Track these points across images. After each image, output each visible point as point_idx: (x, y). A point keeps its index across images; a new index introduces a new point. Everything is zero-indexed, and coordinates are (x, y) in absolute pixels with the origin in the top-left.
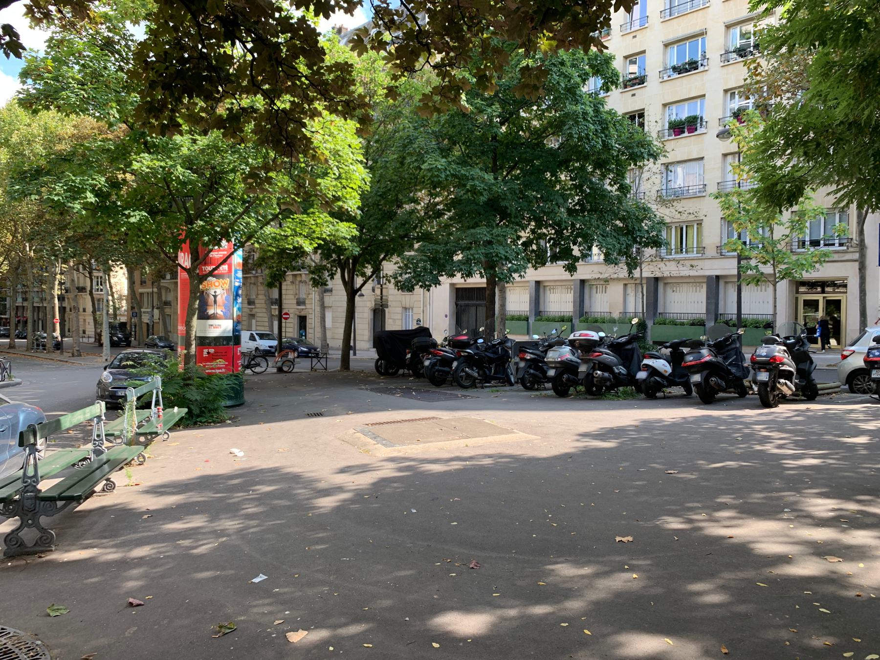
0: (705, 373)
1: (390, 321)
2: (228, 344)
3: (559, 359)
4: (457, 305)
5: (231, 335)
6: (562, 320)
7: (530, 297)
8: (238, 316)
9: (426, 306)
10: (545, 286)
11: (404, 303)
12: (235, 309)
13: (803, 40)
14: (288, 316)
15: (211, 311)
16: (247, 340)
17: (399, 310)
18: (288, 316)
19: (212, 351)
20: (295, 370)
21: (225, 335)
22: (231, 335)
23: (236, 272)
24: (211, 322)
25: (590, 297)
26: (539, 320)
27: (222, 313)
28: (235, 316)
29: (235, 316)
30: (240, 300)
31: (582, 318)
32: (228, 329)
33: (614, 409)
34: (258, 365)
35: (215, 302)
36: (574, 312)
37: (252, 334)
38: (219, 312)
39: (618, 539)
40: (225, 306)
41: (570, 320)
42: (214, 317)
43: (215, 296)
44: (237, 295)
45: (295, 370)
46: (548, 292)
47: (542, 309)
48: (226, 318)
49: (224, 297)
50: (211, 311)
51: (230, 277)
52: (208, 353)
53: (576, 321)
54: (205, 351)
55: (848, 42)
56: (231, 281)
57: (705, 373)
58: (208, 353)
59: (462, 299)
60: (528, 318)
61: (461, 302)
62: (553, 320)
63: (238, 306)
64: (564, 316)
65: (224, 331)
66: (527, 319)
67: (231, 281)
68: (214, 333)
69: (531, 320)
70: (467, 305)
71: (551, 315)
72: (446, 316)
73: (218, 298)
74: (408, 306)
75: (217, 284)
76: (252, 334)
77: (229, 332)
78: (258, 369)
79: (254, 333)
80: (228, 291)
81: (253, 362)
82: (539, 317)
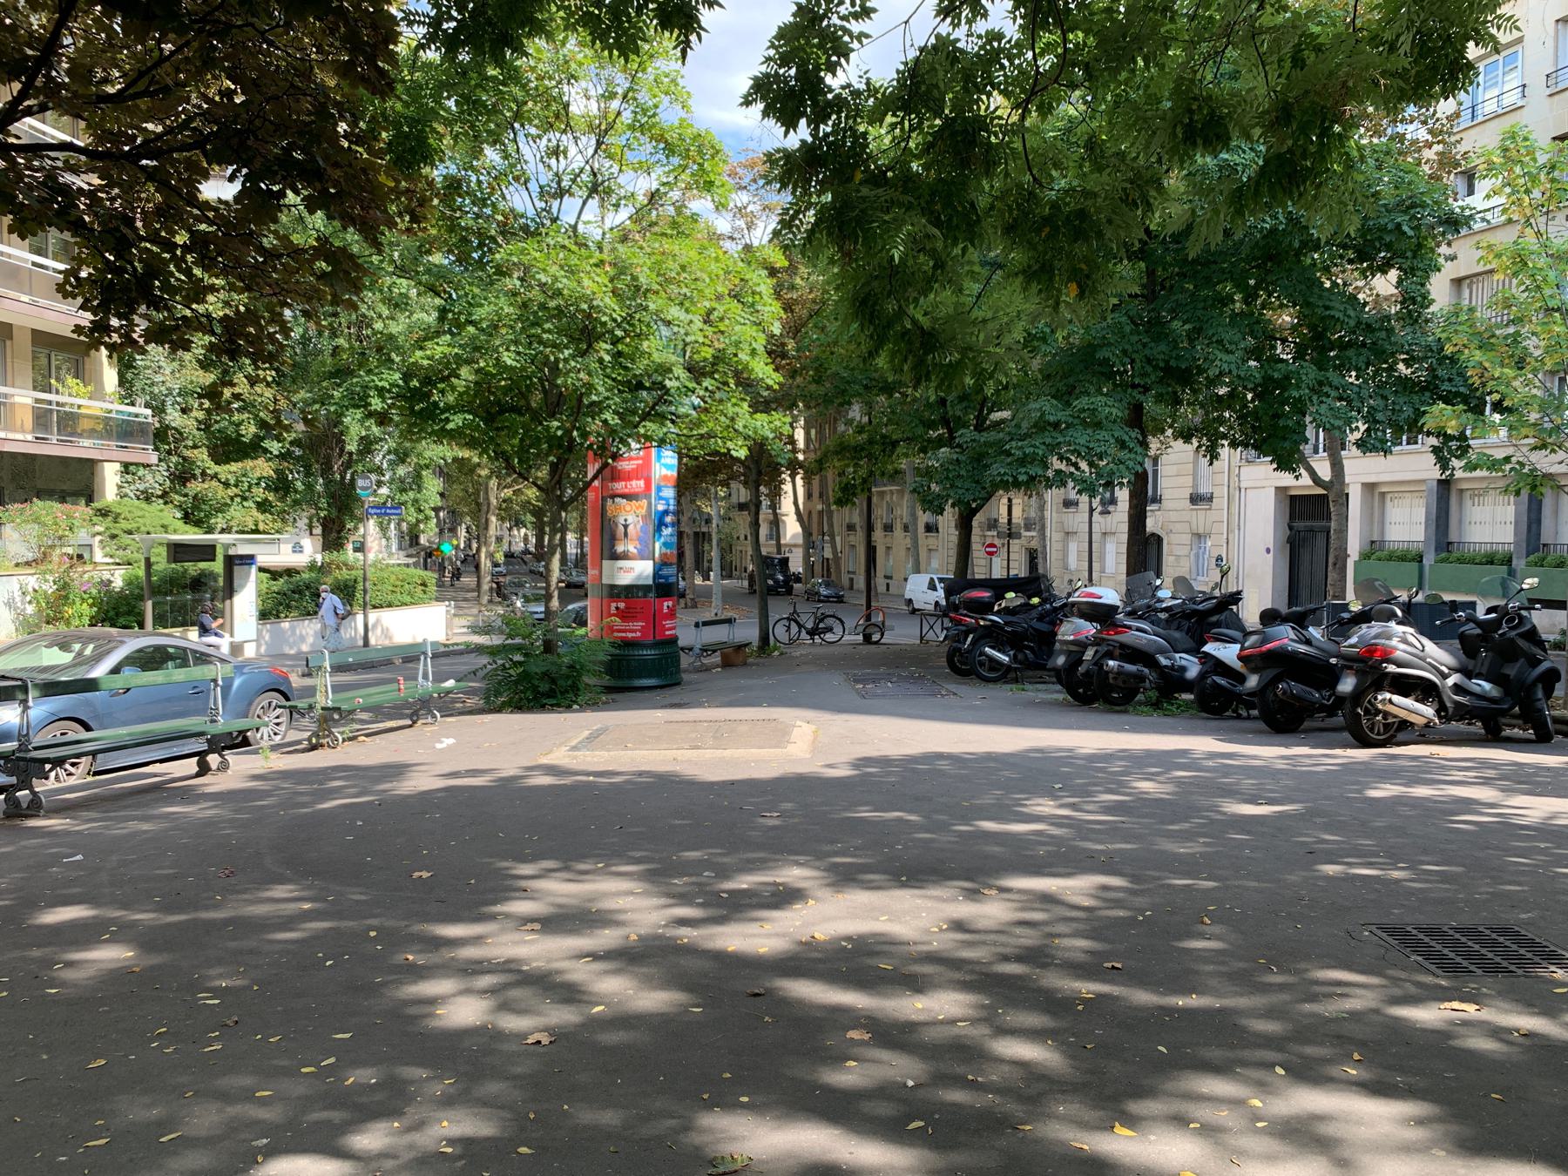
0: (1271, 673)
1: (1171, 559)
2: (645, 596)
3: (1072, 638)
4: (1291, 528)
5: (650, 582)
6: (1490, 560)
7: (1427, 513)
8: (663, 555)
9: (1233, 531)
10: (1461, 491)
11: (1194, 527)
12: (657, 545)
13: (591, 151)
14: (988, 550)
15: (620, 548)
16: (925, 589)
17: (1187, 538)
18: (988, 550)
19: (622, 605)
20: (883, 641)
21: (640, 583)
22: (650, 582)
23: (659, 489)
24: (621, 563)
25: (1556, 512)
26: (1443, 561)
27: (635, 551)
28: (657, 555)
29: (657, 555)
30: (667, 531)
31: (1532, 558)
32: (646, 574)
33: (1079, 728)
34: (830, 630)
35: (626, 534)
36: (1516, 543)
37: (932, 579)
38: (632, 548)
39: (416, 874)
40: (639, 539)
41: (1508, 561)
42: (625, 556)
43: (626, 527)
44: (661, 524)
45: (883, 641)
46: (1468, 502)
47: (1453, 537)
48: (643, 558)
49: (638, 527)
50: (620, 548)
51: (648, 498)
52: (617, 608)
53: (1519, 563)
54: (614, 605)
55: (308, 219)
56: (650, 504)
57: (1271, 673)
58: (617, 608)
59: (1301, 518)
60: (1421, 557)
61: (1299, 525)
62: (1472, 561)
63: (662, 540)
64: (1497, 552)
65: (639, 577)
66: (1419, 558)
67: (650, 504)
68: (625, 579)
69: (1428, 561)
70: (1311, 530)
71: (1468, 551)
72: (1268, 551)
73: (630, 529)
74: (1201, 531)
75: (628, 508)
76: (932, 579)
77: (647, 577)
78: (829, 637)
79: (935, 577)
80: (646, 517)
81: (821, 625)
82: (1444, 555)
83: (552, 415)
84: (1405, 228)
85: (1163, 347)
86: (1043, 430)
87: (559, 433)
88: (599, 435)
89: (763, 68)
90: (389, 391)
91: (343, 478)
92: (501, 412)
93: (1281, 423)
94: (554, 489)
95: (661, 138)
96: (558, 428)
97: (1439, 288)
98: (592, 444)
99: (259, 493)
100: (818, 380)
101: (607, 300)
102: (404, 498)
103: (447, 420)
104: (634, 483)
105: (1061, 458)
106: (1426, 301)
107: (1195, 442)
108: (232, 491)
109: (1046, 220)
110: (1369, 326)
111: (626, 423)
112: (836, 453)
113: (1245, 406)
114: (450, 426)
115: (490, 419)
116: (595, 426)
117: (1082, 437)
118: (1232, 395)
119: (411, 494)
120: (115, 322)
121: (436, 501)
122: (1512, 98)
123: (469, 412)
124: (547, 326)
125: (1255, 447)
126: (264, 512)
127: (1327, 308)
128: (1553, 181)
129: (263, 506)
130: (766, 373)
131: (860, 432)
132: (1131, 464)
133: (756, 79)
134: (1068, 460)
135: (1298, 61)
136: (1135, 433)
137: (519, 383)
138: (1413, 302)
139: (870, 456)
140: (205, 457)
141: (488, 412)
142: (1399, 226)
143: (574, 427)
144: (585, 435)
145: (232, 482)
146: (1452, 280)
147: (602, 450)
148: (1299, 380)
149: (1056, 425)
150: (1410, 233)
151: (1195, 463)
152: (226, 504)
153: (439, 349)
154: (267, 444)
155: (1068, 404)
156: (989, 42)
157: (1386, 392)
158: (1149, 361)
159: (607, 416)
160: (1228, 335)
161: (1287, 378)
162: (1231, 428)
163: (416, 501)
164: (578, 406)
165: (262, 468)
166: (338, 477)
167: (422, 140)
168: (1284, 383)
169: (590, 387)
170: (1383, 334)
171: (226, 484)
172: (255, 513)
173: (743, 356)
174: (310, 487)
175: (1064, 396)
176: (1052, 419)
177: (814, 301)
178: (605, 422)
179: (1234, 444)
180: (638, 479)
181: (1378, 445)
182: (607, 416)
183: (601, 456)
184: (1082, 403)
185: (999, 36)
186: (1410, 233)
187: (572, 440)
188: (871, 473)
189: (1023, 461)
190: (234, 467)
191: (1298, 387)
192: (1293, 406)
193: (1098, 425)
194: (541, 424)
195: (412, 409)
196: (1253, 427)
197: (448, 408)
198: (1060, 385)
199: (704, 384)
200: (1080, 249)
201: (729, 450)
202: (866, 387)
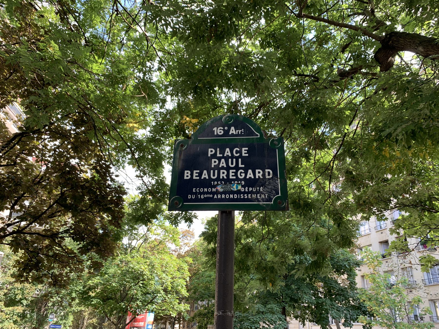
83: (122, 301)
84: (347, 266)
85: (290, 291)
86: (259, 313)
87: (124, 307)
88: (135, 308)
89: (205, 230)
90: (78, 291)
91: (43, 314)
92: (108, 299)
93: (322, 316)
94: (118, 324)
95: (165, 229)
96: (124, 305)
97: (358, 280)
98: (133, 311)
99: (15, 317)
100: (195, 293)
101: (147, 272)
102: (61, 322)
103: (92, 301)
104: (141, 323)
105: (264, 322)
106: (355, 284)
107: (298, 319)
108: (7, 316)
109: (265, 268)
110: (342, 290)
111: (143, 305)
112: (199, 315)
113: (312, 310)
114: (93, 303)
115: (104, 301)
116: (134, 305)
117: (270, 316)
118: (308, 306)
119: (64, 321)
120: (25, 274)
121: (71, 324)
122: (368, 231)
123: (99, 299)
124: (128, 276)
125: (317, 323)
126: (15, 324)
127: (331, 284)
128: (378, 260)
129: (15, 322)
130: (184, 293)
131: (205, 309)
132: (283, 325)
133: (203, 232)
134: (266, 323)
135: (317, 239)
136: (284, 317)
137: (114, 291)
138: (352, 285)
139: (207, 318)
140: (3, 305)
141: (103, 299)
142: (345, 265)
143: (129, 305)
144: (131, 308)
145: (8, 313)
146: (361, 276)
147: (135, 313)
148: (326, 303)
149: (262, 313)
150: (348, 267)
151: (299, 324)
152: (4, 321)
153: (96, 280)
154: (22, 301)
155: (265, 306)
156: (252, 227)
157: (349, 309)
158: (287, 295)
159: (138, 302)
160: (306, 290)
161: (323, 303)
162: (309, 316)
163: (65, 323)
164: (133, 299)
165: (19, 309)
166: (42, 313)
167: (119, 235)
168: (322, 304)
169: (136, 294)
170: (346, 292)
171: (7, 314)
172: (12, 324)
173: (180, 288)
174: (31, 317)
175: (265, 304)
176: (261, 310)
177: (195, 270)
178: (137, 304)
179: (310, 321)
180: (142, 322)
181: (348, 325)
182: (138, 302)
183: (134, 314)
184: (269, 306)
185: (254, 227)
186: (348, 267)
187: (127, 309)
188: (208, 322)
189: (253, 323)
190: (11, 308)
191: (326, 306)
192: (325, 311)
193: (273, 313)
194: (118, 304)
195: (82, 297)
196: (315, 316)
197: (93, 297)
198: (263, 301)
199: (169, 296)
200: (272, 275)
201: (170, 314)
202: (209, 296)
